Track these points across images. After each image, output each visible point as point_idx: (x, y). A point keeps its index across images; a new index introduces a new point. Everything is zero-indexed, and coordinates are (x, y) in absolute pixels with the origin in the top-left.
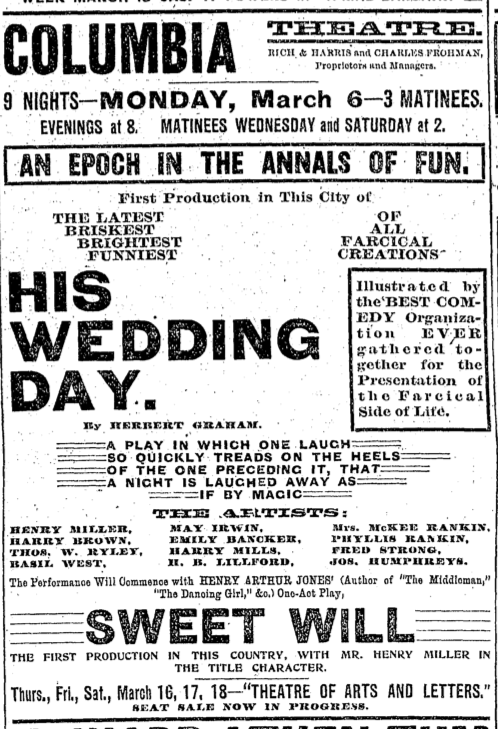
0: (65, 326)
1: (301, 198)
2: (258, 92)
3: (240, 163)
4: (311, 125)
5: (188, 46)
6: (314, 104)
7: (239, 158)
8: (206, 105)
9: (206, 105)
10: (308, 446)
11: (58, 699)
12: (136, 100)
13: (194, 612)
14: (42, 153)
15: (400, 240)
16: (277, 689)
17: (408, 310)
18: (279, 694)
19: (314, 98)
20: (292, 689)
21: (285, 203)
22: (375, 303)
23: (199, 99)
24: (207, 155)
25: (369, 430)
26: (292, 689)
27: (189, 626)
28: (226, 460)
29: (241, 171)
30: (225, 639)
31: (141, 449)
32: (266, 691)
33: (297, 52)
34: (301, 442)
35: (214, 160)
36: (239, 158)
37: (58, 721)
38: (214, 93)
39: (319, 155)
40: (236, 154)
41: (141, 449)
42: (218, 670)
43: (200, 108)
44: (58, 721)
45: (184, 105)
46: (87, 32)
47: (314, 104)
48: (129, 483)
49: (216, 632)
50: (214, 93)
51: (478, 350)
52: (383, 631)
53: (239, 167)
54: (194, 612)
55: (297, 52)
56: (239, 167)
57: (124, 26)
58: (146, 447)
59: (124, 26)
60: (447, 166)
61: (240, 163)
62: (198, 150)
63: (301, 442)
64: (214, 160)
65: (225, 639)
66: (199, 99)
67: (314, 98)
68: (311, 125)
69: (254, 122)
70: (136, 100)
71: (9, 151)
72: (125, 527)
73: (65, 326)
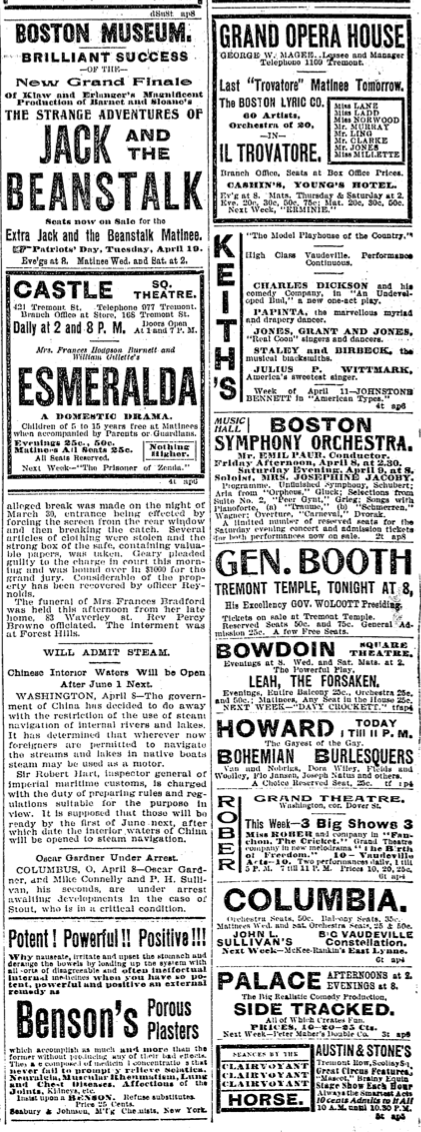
2: (325, 890)
6: (302, 984)
11: (134, 158)
12: (246, 728)
15: (365, 566)
19: (302, 976)
23: (387, 900)
28: (307, 1013)
30: (318, 988)
31: (265, 987)
32: (355, 35)
37: (55, 7)
41: (265, 987)
44: (55, 7)
47: (302, 984)
57: (320, 890)
58: (273, 984)
59: (320, 890)
65: (318, 988)
66: (387, 900)
67: (302, 976)
69: (395, 753)
70: (246, 728)
72: (406, 732)
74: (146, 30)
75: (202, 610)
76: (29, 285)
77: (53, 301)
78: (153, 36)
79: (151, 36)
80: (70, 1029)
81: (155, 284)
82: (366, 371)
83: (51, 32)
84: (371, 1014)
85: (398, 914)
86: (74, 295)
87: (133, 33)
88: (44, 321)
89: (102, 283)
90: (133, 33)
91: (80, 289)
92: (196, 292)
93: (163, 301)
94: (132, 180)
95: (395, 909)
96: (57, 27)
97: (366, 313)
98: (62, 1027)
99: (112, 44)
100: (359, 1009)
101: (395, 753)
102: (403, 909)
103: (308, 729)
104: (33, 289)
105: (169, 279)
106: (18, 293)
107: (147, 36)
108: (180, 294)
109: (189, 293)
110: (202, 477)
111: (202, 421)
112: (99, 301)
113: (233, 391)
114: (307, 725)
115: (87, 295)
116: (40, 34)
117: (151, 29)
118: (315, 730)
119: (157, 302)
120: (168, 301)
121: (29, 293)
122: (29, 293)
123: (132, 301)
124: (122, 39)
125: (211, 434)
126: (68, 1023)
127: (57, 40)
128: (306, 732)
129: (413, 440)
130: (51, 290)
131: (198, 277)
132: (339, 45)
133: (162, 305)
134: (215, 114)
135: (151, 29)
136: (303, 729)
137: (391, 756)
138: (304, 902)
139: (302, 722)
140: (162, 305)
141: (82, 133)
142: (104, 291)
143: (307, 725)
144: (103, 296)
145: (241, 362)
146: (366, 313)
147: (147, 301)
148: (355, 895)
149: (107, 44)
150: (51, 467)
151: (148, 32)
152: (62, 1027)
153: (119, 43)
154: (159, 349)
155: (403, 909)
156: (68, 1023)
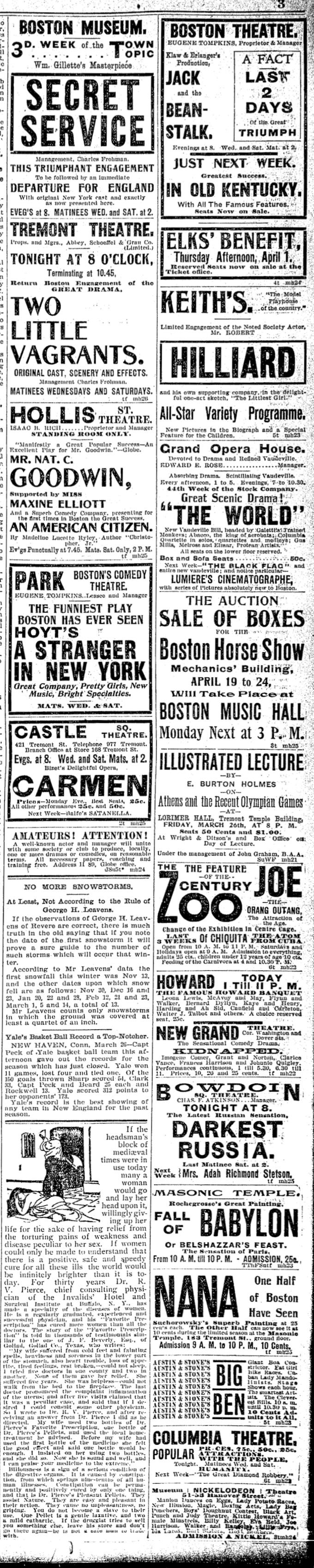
0: (94, 118)
3: (208, 515)
5: (226, 1374)
7: (207, 511)
8: (267, 111)
9: (267, 111)
10: (255, 78)
24: (237, 27)
25: (178, 218)
29: (209, 523)
34: (248, 74)
35: (241, 29)
36: (207, 511)
38: (272, 104)
40: (289, 26)
43: (263, 113)
45: (254, 111)
50: (272, 104)
52: (59, 418)
53: (207, 519)
56: (207, 519)
61: (208, 515)
62: (231, 24)
63: (248, 74)
64: (241, 29)
71: (16, 78)
73: (94, 118)
76: (30, 781)
77: (43, 740)
81: (119, 728)
83: (45, 27)
85: (269, 1161)
86: (58, 736)
87: (104, 28)
88: (38, 754)
89: (78, 727)
90: (104, 28)
91: (62, 731)
92: (148, 733)
93: (123, 739)
94: (279, 1126)
95: (265, 1157)
96: (49, 23)
99: (89, 36)
100: (235, 1128)
102: (272, 1156)
103: (213, 1129)
104: (29, 732)
105: (130, 725)
106: (18, 736)
108: (135, 735)
109: (141, 735)
110: (149, 819)
111: (151, 591)
112: (76, 740)
114: (212, 1126)
115: (67, 736)
119: (118, 741)
120: (127, 740)
121: (26, 735)
122: (26, 735)
123: (101, 739)
124: (97, 32)
125: (156, 49)
127: (49, 32)
128: (211, 1133)
129: (309, 413)
130: (41, 733)
133: (122, 743)
136: (208, 1129)
138: (202, 1152)
140: (122, 743)
141: (72, 86)
142: (80, 733)
143: (212, 1126)
144: (79, 736)
147: (111, 740)
149: (86, 36)
150: (47, 813)
151: (115, 28)
153: (95, 35)
155: (272, 1156)
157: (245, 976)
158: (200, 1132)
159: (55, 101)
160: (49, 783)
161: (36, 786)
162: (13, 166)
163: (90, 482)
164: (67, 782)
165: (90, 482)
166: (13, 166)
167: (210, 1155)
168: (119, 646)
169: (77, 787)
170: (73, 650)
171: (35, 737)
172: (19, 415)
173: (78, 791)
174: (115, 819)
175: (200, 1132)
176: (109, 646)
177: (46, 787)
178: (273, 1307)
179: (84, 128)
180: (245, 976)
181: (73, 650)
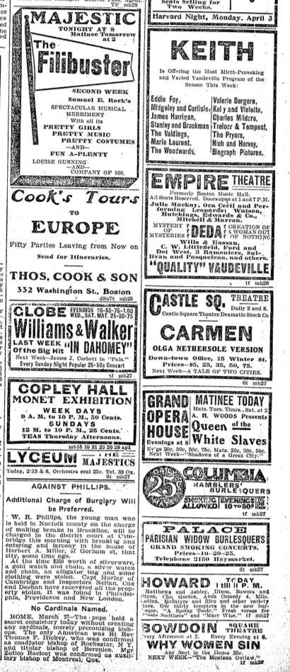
1: (211, 441)
4: (262, 401)
13: (205, 43)
14: (256, 623)
16: (248, 178)
17: (98, 138)
18: (250, 182)
20: (259, 178)
21: (65, 234)
22: (51, 45)
26: (259, 178)
27: (203, 50)
33: (39, 471)
39: (70, 462)
42: (227, 57)
46: (235, 431)
48: (211, 658)
49: (46, 459)
51: (132, 247)
54: (205, 43)
55: (39, 471)
60: (209, 629)
68: (262, 401)
74: (184, 430)
75: (6, 587)
78: (205, 234)
79: (203, 234)
80: (68, 334)
82: (114, 142)
84: (204, 58)
90: (174, 432)
92: (270, 199)
97: (255, 315)
98: (64, 334)
101: (255, 538)
107: (184, 434)
113: (244, 645)
116: (213, 301)
117: (204, 229)
118: (199, 584)
126: (66, 331)
128: (197, 336)
131: (133, 385)
132: (210, 264)
134: (9, 408)
135: (204, 229)
136: (194, 334)
137: (253, 539)
139: (194, 327)
145: (140, 32)
146: (255, 315)
148: (197, 330)
152: (64, 334)
154: (128, 248)
156: (66, 331)
157: (228, 579)
158: (186, 335)
159: (119, 350)
160: (185, 330)
161: (176, 333)
162: (14, 273)
163: (197, 441)
164: (197, 330)
165: (197, 441)
166: (14, 273)
167: (213, 297)
168: (169, 414)
169: (204, 334)
170: (164, 401)
171: (183, 339)
172: (92, 390)
173: (204, 337)
174: (65, 442)
175: (186, 335)
176: (154, 399)
177: (183, 333)
178: (52, 362)
179: (117, 335)
180: (228, 579)
181: (164, 401)
